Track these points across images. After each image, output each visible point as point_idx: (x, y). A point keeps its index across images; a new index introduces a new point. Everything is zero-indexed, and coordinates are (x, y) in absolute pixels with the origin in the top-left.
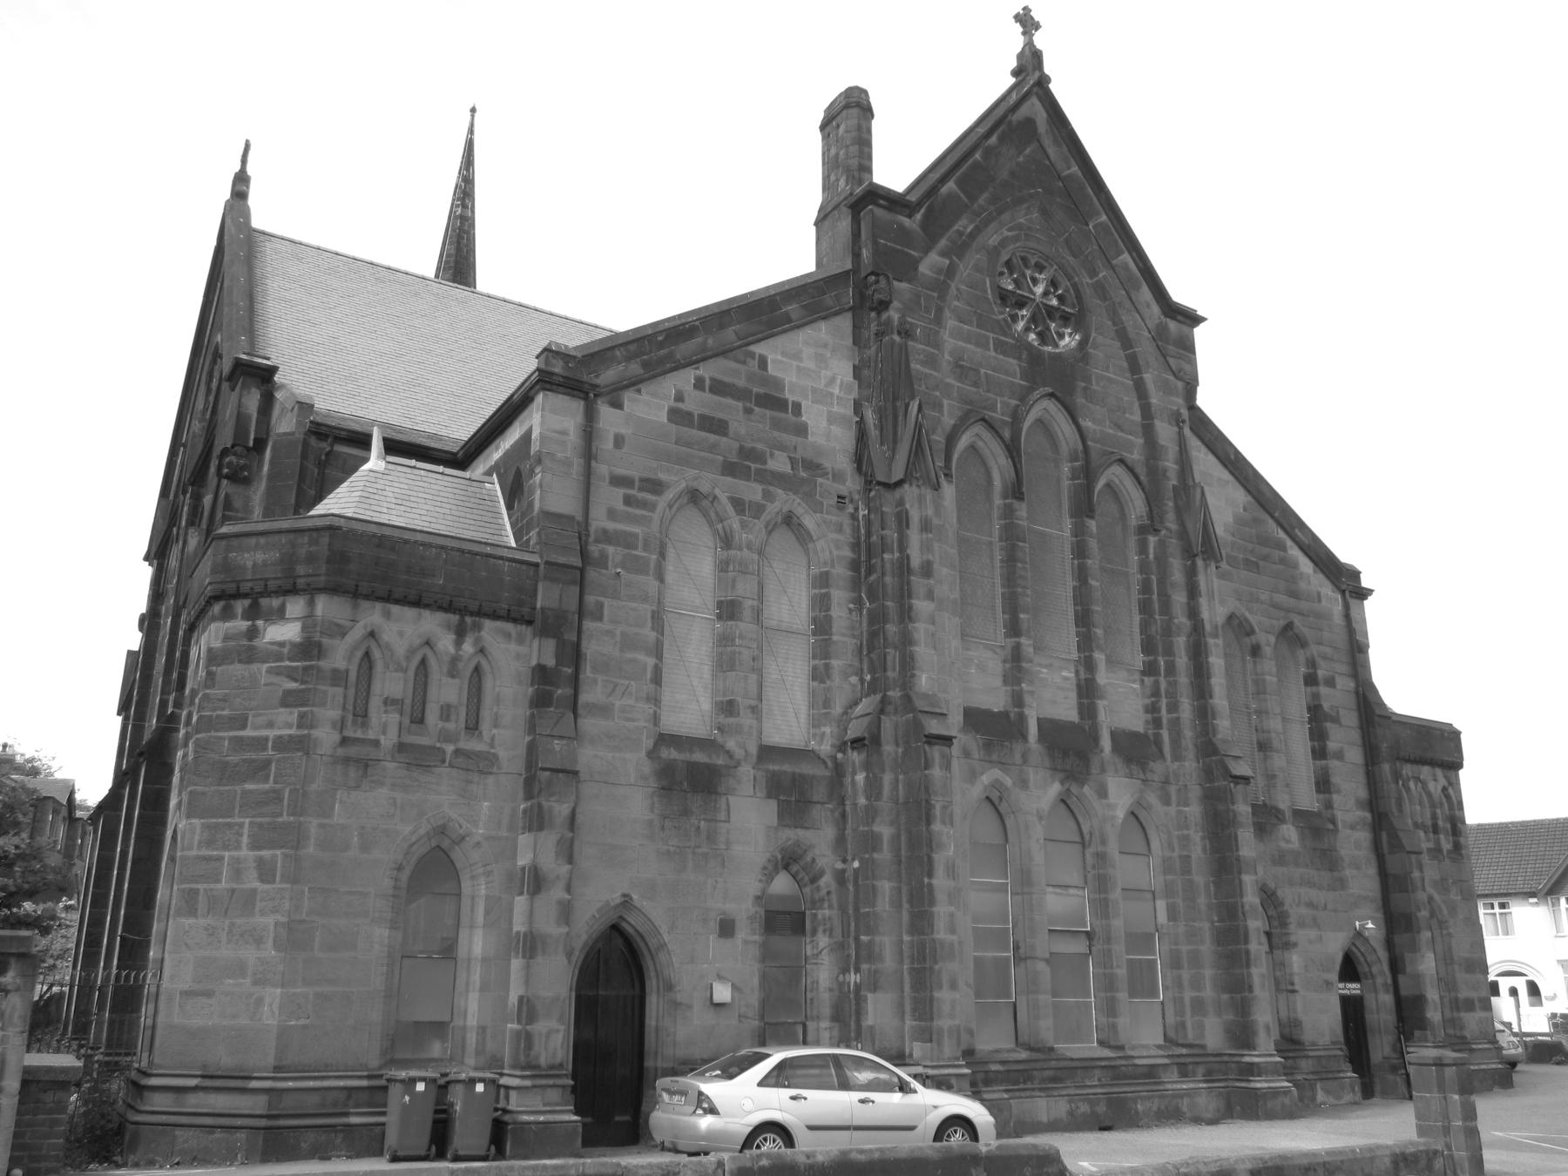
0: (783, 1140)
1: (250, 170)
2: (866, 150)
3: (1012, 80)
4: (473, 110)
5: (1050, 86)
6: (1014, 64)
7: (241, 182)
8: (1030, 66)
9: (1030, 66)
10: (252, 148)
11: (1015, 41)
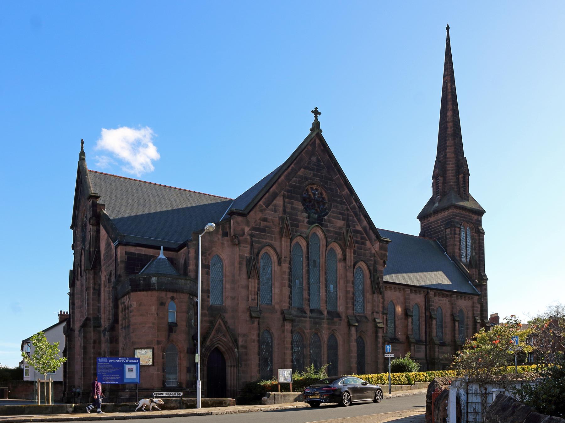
2: (454, 86)
4: (448, 28)
7: (82, 154)
8: (316, 125)
9: (316, 125)
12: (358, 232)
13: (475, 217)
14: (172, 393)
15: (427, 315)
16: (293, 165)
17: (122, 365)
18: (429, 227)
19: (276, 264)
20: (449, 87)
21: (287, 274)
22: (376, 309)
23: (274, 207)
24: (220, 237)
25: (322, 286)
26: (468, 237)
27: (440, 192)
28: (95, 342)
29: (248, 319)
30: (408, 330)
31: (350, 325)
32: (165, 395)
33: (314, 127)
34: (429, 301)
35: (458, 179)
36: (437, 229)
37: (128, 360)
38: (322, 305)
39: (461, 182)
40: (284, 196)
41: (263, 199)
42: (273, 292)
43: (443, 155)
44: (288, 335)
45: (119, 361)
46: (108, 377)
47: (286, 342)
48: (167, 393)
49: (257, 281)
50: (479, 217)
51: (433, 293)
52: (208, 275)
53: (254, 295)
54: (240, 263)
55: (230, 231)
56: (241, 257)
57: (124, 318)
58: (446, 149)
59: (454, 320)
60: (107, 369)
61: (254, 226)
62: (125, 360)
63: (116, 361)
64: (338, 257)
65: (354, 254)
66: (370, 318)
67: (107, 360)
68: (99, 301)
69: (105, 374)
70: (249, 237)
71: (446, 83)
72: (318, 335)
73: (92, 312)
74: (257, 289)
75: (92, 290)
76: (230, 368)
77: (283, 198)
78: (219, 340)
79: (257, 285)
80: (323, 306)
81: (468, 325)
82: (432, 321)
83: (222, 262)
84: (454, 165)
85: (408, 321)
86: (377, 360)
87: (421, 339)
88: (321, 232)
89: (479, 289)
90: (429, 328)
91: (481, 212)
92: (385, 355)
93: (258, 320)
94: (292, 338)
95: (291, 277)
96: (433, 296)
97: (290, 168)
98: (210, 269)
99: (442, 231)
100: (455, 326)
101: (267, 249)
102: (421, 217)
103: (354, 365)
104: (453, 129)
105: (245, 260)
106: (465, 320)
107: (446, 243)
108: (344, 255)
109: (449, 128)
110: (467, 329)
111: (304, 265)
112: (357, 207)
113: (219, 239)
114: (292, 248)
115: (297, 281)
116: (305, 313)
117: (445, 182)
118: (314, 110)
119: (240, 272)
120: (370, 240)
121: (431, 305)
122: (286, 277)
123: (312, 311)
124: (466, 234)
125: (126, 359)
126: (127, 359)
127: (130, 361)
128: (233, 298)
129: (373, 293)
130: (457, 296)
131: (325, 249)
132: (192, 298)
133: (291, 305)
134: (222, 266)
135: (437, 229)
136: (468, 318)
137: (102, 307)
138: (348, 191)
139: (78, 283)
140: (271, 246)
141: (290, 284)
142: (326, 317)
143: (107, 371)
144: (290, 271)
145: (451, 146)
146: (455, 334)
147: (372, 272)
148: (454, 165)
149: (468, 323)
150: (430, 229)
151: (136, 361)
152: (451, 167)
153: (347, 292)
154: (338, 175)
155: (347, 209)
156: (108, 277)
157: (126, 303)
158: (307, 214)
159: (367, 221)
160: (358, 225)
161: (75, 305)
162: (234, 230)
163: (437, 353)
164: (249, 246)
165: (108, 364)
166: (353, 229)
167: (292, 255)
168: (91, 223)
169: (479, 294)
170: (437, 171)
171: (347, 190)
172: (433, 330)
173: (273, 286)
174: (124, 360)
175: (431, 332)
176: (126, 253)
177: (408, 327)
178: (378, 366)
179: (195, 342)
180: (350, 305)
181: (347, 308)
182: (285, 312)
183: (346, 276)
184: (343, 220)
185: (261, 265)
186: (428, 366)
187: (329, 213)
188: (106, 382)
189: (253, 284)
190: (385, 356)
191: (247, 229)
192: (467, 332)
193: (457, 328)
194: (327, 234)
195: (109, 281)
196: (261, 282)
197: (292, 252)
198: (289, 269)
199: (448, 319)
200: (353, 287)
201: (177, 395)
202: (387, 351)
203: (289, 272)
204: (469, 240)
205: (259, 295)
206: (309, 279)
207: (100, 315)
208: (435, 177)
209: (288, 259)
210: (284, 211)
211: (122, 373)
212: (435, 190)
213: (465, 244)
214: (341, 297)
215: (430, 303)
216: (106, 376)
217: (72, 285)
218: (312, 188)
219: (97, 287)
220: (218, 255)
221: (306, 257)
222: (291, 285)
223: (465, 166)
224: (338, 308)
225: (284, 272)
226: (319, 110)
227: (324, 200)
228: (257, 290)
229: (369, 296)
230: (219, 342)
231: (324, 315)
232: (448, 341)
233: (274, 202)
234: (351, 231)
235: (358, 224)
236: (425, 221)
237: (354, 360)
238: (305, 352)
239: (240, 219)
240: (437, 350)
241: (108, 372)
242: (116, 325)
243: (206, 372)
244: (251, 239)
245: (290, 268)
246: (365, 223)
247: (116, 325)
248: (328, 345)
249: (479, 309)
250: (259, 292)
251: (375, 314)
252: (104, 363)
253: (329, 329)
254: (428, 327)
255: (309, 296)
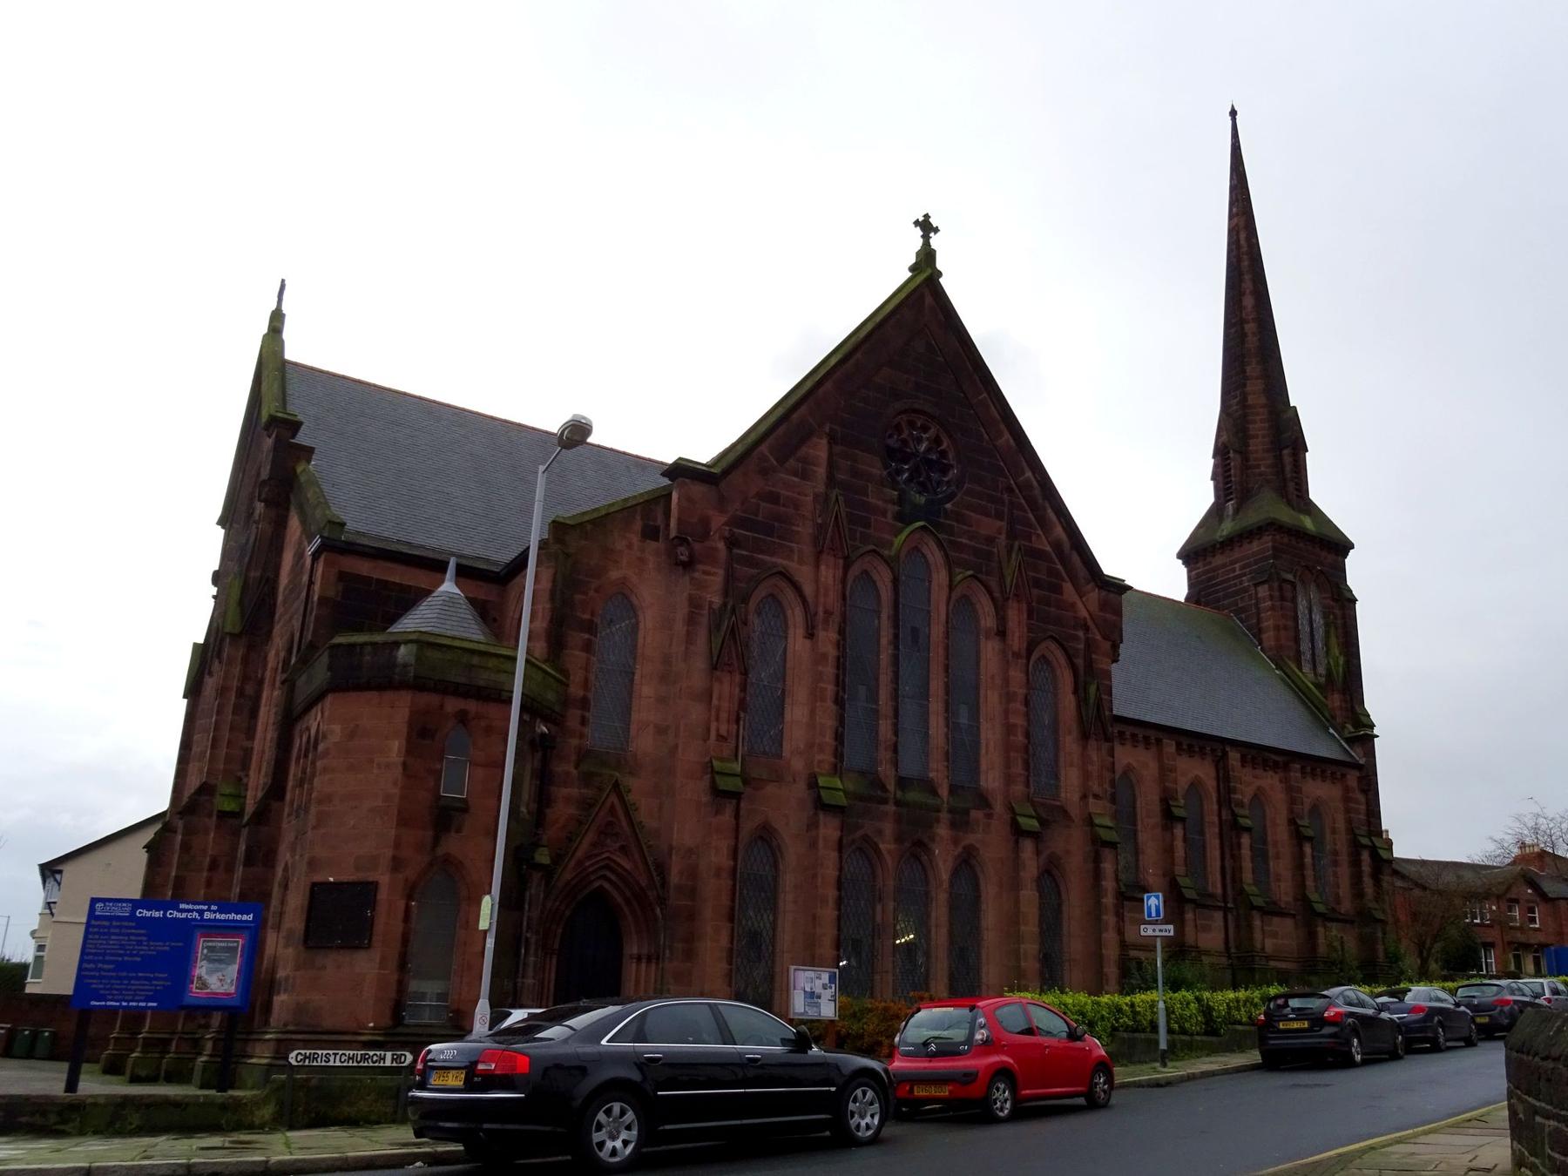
0: (639, 1135)
1: (285, 309)
2: (1254, 241)
3: (910, 274)
4: (1233, 113)
5: (941, 280)
6: (912, 260)
7: (277, 318)
8: (926, 258)
9: (926, 258)
10: (286, 287)
11: (915, 239)
12: (1039, 554)
13: (1331, 558)
14: (371, 1053)
15: (1224, 818)
16: (859, 355)
17: (186, 932)
18: (1210, 579)
19: (800, 631)
20: (1243, 242)
21: (831, 660)
22: (1096, 788)
23: (800, 465)
24: (636, 539)
25: (936, 706)
26: (1315, 608)
27: (1236, 489)
28: (213, 866)
29: (705, 799)
30: (1173, 859)
31: (1018, 832)
32: (338, 1064)
33: (921, 260)
34: (1227, 779)
35: (1279, 458)
36: (1230, 587)
37: (215, 912)
38: (933, 765)
39: (1288, 468)
40: (832, 440)
41: (771, 440)
42: (788, 716)
43: (1238, 399)
44: (830, 858)
45: (179, 915)
46: (120, 978)
47: (820, 880)
48: (347, 1052)
49: (738, 678)
50: (1340, 558)
51: (1239, 755)
52: (587, 652)
53: (729, 721)
54: (691, 620)
55: (668, 525)
56: (694, 604)
57: (301, 778)
58: (1245, 385)
59: (1299, 838)
60: (122, 947)
61: (738, 513)
62: (201, 912)
63: (164, 914)
64: (983, 622)
65: (1030, 616)
66: (1074, 812)
67: (129, 909)
68: (250, 733)
69: (111, 966)
70: (721, 545)
71: (1235, 233)
72: (919, 860)
73: (222, 767)
74: (736, 706)
75: (233, 698)
76: (634, 965)
77: (829, 443)
78: (607, 867)
79: (737, 690)
80: (937, 771)
81: (1336, 853)
82: (1239, 837)
83: (636, 616)
84: (1267, 425)
85: (1173, 834)
86: (1101, 949)
87: (1210, 889)
88: (935, 547)
89: (1359, 750)
90: (1233, 856)
91: (1344, 546)
92: (1142, 927)
93: (734, 801)
94: (841, 869)
95: (844, 675)
96: (1239, 764)
97: (852, 361)
98: (596, 636)
99: (1246, 590)
100: (1301, 855)
101: (776, 585)
102: (1190, 555)
103: (1031, 965)
104: (1258, 337)
105: (705, 612)
106: (1328, 836)
107: (1259, 621)
108: (1002, 619)
109: (1250, 334)
110: (1335, 863)
111: (884, 641)
112: (1035, 483)
113: (630, 546)
114: (849, 586)
115: (862, 690)
116: (884, 788)
117: (1246, 465)
118: (921, 219)
119: (687, 648)
120: (1073, 579)
121: (1235, 791)
122: (829, 670)
123: (902, 782)
124: (1310, 602)
125: (206, 907)
126: (209, 910)
127: (223, 917)
128: (661, 731)
129: (1085, 736)
130: (1303, 768)
131: (944, 598)
132: (528, 719)
133: (842, 761)
134: (635, 628)
135: (1230, 587)
136: (1334, 831)
137: (255, 752)
138: (1012, 441)
139: (210, 684)
140: (786, 576)
141: (841, 693)
142: (945, 805)
143: (120, 955)
144: (841, 654)
145: (1257, 378)
146: (1303, 876)
147: (1082, 672)
148: (1267, 425)
149: (1337, 847)
150: (1214, 585)
151: (245, 917)
152: (1259, 427)
153: (1009, 729)
154: (982, 393)
155: (1010, 490)
156: (282, 654)
157: (313, 732)
158: (896, 493)
159: (1063, 527)
160: (1038, 535)
161: (191, 750)
162: (680, 521)
163: (1258, 935)
164: (721, 572)
165: (131, 928)
166: (1024, 545)
167: (848, 608)
168: (263, 496)
169: (1361, 762)
170: (1225, 437)
171: (1007, 435)
172: (1243, 864)
173: (788, 700)
174: (197, 911)
175: (1237, 870)
176: (342, 576)
177: (1173, 853)
178: (1105, 970)
179: (525, 867)
180: (1018, 769)
181: (1009, 779)
182: (822, 781)
183: (1006, 681)
184: (999, 516)
185: (754, 632)
186: (1234, 975)
187: (959, 495)
188: (109, 1003)
189: (726, 688)
190: (1143, 933)
191: (718, 521)
192: (1335, 874)
193: (1308, 860)
194: (951, 553)
195: (286, 661)
196: (752, 683)
197: (848, 599)
198: (839, 648)
199: (1280, 833)
200: (1027, 715)
201: (388, 1063)
202: (1149, 915)
203: (838, 658)
204: (1318, 618)
205: (741, 723)
206: (897, 684)
207: (247, 776)
208: (1221, 452)
209: (836, 618)
210: (831, 481)
211: (180, 964)
212: (1221, 485)
213: (1307, 629)
214: (992, 743)
215: (1232, 784)
216: (114, 974)
217: (193, 690)
218: (911, 424)
219: (249, 689)
220: (623, 594)
221: (889, 617)
222: (842, 697)
223: (1295, 428)
224: (983, 777)
225: (824, 656)
226: (934, 222)
227: (945, 459)
228: (736, 709)
229: (1070, 743)
230: (608, 874)
231: (939, 796)
232: (1284, 898)
233: (804, 450)
234: (1020, 549)
235: (1040, 532)
236: (1200, 564)
237: (1030, 948)
238: (879, 918)
239: (698, 489)
240: (1257, 923)
241: (126, 958)
242: (275, 805)
243: (553, 976)
244: (729, 549)
245: (840, 645)
246: (1059, 531)
247: (275, 805)
248: (951, 894)
249: (1363, 807)
250: (742, 715)
251: (1091, 800)
252: (114, 923)
253: (956, 842)
254: (1228, 856)
255: (896, 733)
